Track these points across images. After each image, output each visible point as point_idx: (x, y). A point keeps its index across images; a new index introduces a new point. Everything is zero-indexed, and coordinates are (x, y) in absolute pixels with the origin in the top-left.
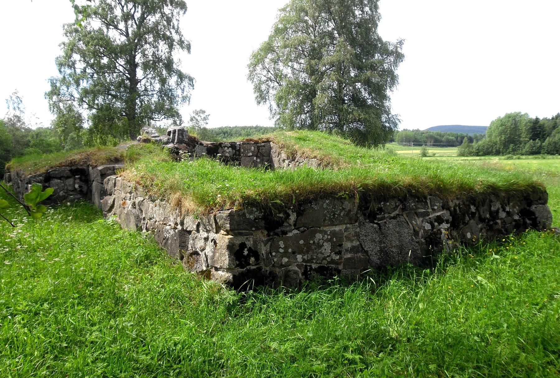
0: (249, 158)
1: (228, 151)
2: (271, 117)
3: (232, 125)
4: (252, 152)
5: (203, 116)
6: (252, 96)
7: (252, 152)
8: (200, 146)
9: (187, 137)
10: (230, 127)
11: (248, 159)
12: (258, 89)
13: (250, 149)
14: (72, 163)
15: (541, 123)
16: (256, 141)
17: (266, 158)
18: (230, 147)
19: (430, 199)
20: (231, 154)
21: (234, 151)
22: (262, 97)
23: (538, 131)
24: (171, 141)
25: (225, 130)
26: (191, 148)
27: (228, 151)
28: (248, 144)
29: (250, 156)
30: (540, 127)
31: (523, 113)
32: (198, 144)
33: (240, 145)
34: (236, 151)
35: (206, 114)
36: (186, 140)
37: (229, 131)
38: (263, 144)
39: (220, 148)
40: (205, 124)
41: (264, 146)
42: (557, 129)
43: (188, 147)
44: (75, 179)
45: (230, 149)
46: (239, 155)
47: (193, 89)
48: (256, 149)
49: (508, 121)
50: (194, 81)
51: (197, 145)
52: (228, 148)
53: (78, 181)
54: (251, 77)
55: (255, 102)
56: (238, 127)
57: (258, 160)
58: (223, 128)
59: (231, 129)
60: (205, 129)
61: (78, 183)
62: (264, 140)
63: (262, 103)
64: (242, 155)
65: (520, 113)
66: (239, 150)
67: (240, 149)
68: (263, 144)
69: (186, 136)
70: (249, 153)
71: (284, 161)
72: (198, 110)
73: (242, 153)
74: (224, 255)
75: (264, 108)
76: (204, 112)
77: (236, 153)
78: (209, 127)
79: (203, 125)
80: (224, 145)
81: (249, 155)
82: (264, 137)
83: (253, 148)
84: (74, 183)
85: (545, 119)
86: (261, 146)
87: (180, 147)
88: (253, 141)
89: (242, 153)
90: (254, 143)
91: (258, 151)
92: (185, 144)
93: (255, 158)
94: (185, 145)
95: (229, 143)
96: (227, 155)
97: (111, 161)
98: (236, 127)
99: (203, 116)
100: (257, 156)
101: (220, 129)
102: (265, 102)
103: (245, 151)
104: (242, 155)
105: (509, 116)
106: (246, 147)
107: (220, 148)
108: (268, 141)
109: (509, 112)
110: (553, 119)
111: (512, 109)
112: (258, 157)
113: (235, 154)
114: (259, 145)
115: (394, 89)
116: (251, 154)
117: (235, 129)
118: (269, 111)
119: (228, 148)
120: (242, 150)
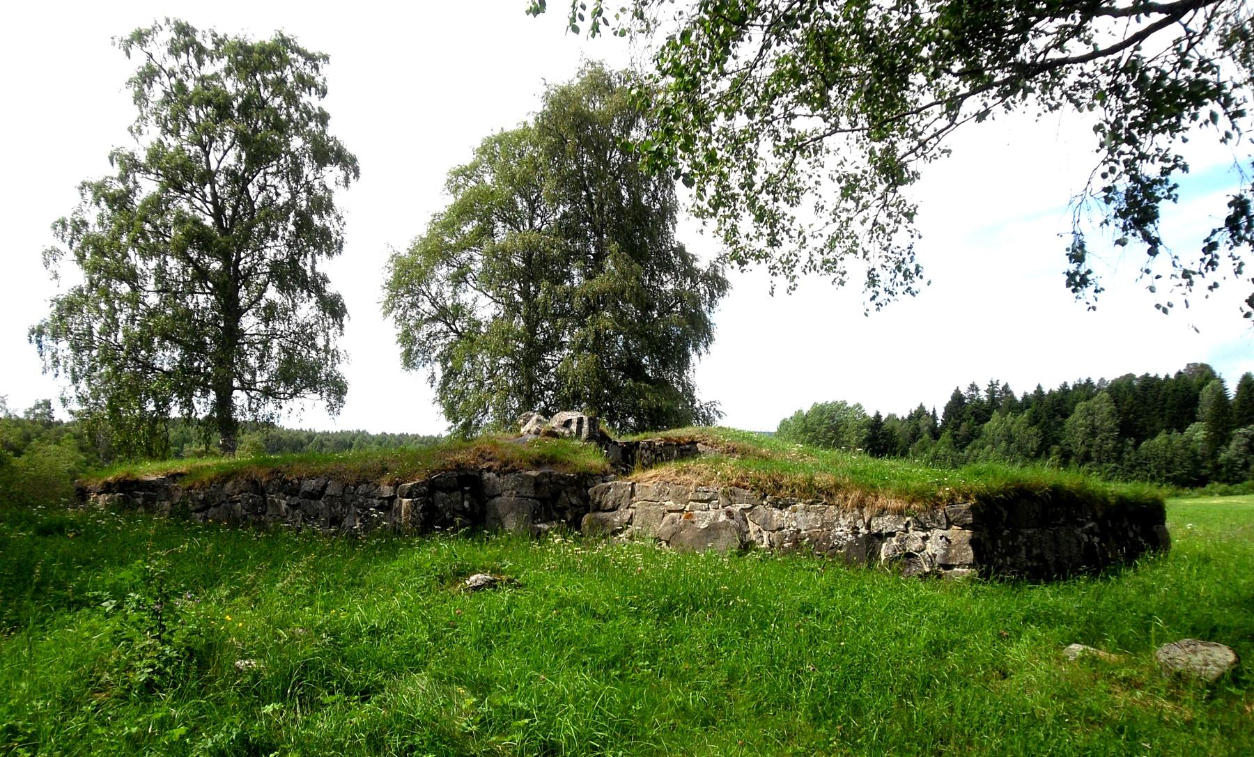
12: (407, 338)
14: (459, 467)
15: (888, 426)
23: (880, 444)
30: (884, 434)
31: (850, 405)
38: (688, 446)
42: (920, 440)
44: (464, 492)
47: (342, 334)
49: (821, 423)
53: (467, 496)
61: (468, 500)
65: (844, 403)
68: (688, 446)
74: (966, 550)
84: (463, 500)
85: (393, 435)
105: (819, 410)
109: (821, 401)
110: (911, 417)
111: (827, 396)
115: (711, 347)
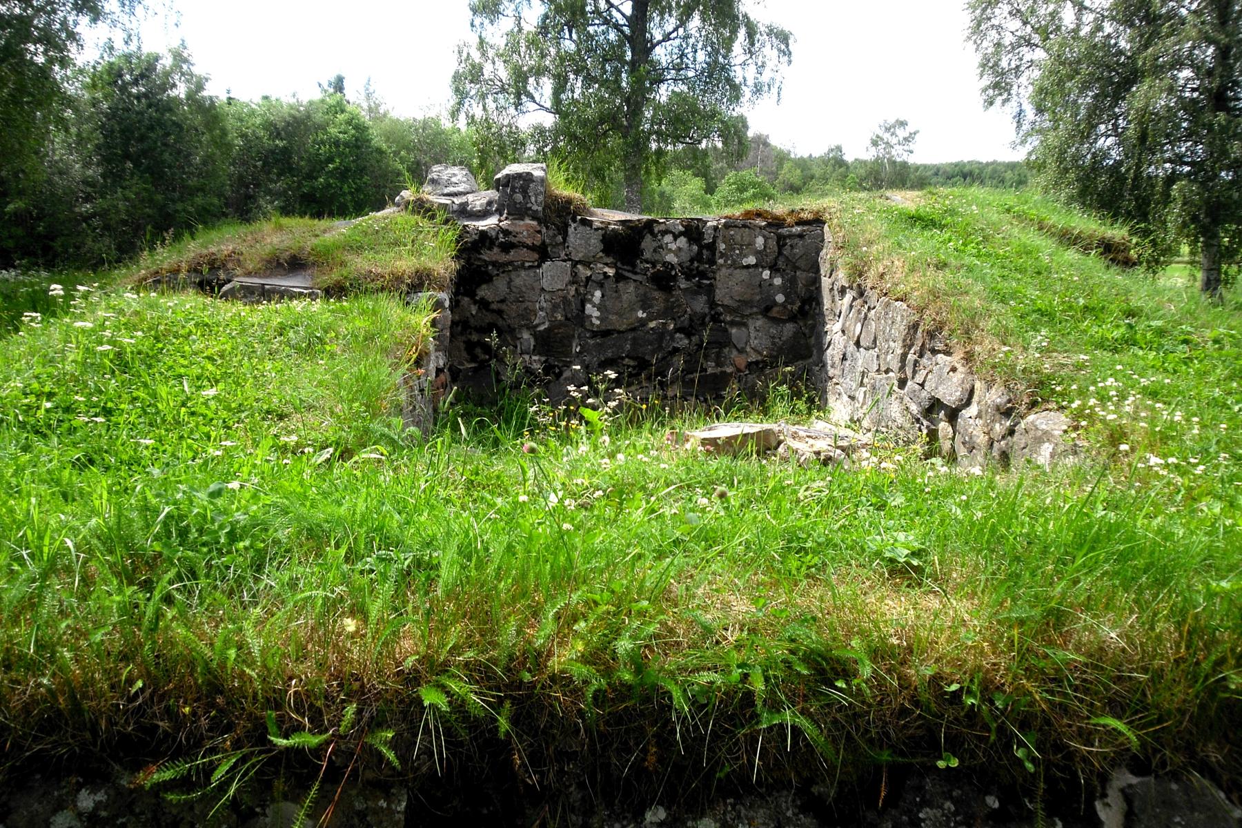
0: (745, 272)
1: (673, 247)
2: (1018, 141)
3: (984, 159)
4: (757, 253)
5: (902, 133)
6: (975, 83)
7: (757, 253)
8: (581, 228)
9: (541, 198)
10: (980, 163)
11: (740, 275)
12: (989, 65)
13: (751, 244)
16: (776, 218)
17: (804, 275)
18: (681, 234)
19: (1127, 795)
20: (685, 257)
21: (695, 248)
22: (1000, 86)
24: (496, 211)
25: (966, 169)
26: (551, 233)
27: (673, 247)
28: (744, 226)
29: (748, 267)
32: (574, 220)
33: (716, 228)
34: (701, 247)
35: (910, 128)
36: (535, 207)
37: (977, 171)
39: (648, 238)
40: (905, 154)
41: (801, 236)
43: (544, 230)
45: (682, 241)
46: (712, 262)
48: (773, 243)
50: (790, 42)
51: (573, 225)
52: (676, 237)
54: (977, 28)
55: (980, 100)
56: (999, 164)
57: (778, 281)
58: (964, 165)
59: (983, 167)
60: (904, 165)
62: (805, 215)
63: (999, 100)
64: (721, 261)
66: (712, 247)
67: (714, 242)
69: (536, 196)
70: (746, 256)
71: (843, 291)
72: (892, 121)
73: (722, 255)
75: (1003, 115)
76: (903, 124)
77: (700, 253)
78: (912, 160)
79: (899, 153)
80: (662, 227)
81: (745, 262)
82: (808, 204)
83: (760, 241)
86: (791, 236)
87: (518, 230)
88: (765, 218)
89: (722, 255)
90: (769, 225)
91: (780, 253)
92: (534, 218)
93: (766, 274)
94: (535, 223)
95: (682, 220)
96: (671, 258)
97: (279, 265)
98: (994, 163)
99: (902, 133)
100: (774, 269)
101: (956, 165)
102: (1007, 100)
103: (734, 249)
104: (721, 261)
106: (738, 238)
107: (648, 238)
108: (818, 221)
112: (778, 270)
113: (698, 257)
114: (784, 231)
116: (752, 260)
117: (990, 168)
118: (1015, 125)
119: (676, 237)
120: (722, 247)
